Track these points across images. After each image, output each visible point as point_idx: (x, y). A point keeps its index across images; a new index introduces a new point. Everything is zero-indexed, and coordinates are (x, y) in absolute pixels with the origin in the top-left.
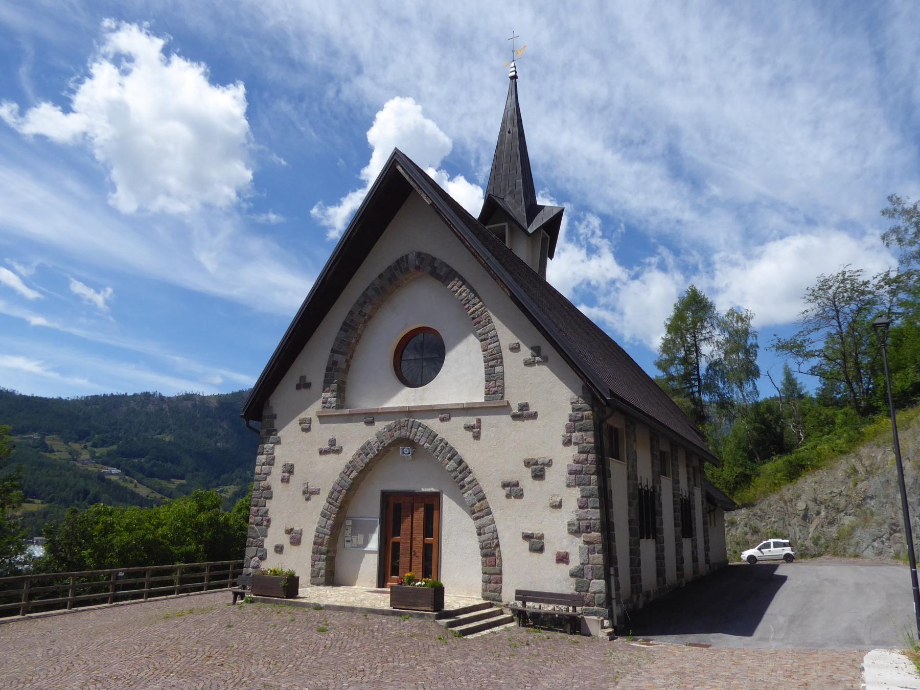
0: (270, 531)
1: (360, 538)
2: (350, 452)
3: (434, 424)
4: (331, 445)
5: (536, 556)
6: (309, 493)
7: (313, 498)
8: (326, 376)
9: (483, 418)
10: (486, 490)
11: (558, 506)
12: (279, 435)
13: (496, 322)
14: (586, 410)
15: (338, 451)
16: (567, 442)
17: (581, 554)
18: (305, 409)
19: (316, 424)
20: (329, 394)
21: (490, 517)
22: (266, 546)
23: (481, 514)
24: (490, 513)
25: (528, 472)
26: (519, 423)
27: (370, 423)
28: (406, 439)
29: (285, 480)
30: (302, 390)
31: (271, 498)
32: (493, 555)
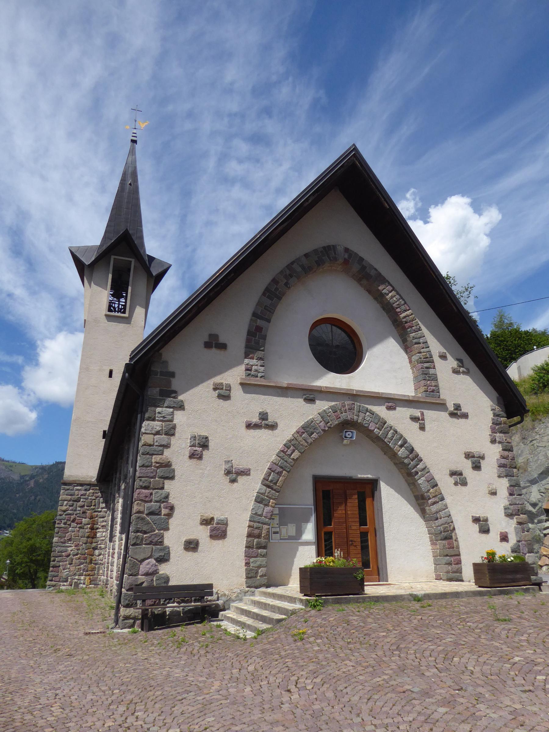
0: (173, 522)
1: (291, 529)
2: (288, 429)
3: (381, 410)
4: (263, 419)
5: (484, 536)
6: (234, 474)
7: (242, 479)
8: (248, 341)
9: (426, 412)
10: (437, 477)
11: (494, 493)
12: (180, 398)
13: (425, 330)
14: (503, 417)
15: (273, 427)
16: (493, 441)
17: (517, 533)
18: (220, 373)
19: (237, 392)
20: (254, 361)
21: (443, 502)
22: (166, 542)
23: (436, 499)
24: (443, 499)
25: (468, 463)
26: (455, 420)
27: (310, 400)
28: (351, 423)
29: (194, 456)
30: (214, 350)
31: (172, 478)
32: (451, 538)
